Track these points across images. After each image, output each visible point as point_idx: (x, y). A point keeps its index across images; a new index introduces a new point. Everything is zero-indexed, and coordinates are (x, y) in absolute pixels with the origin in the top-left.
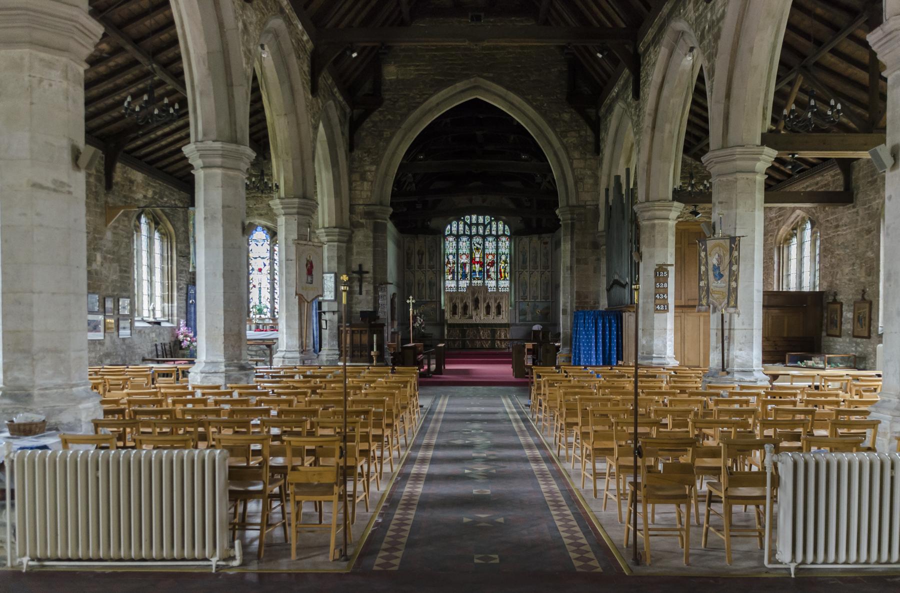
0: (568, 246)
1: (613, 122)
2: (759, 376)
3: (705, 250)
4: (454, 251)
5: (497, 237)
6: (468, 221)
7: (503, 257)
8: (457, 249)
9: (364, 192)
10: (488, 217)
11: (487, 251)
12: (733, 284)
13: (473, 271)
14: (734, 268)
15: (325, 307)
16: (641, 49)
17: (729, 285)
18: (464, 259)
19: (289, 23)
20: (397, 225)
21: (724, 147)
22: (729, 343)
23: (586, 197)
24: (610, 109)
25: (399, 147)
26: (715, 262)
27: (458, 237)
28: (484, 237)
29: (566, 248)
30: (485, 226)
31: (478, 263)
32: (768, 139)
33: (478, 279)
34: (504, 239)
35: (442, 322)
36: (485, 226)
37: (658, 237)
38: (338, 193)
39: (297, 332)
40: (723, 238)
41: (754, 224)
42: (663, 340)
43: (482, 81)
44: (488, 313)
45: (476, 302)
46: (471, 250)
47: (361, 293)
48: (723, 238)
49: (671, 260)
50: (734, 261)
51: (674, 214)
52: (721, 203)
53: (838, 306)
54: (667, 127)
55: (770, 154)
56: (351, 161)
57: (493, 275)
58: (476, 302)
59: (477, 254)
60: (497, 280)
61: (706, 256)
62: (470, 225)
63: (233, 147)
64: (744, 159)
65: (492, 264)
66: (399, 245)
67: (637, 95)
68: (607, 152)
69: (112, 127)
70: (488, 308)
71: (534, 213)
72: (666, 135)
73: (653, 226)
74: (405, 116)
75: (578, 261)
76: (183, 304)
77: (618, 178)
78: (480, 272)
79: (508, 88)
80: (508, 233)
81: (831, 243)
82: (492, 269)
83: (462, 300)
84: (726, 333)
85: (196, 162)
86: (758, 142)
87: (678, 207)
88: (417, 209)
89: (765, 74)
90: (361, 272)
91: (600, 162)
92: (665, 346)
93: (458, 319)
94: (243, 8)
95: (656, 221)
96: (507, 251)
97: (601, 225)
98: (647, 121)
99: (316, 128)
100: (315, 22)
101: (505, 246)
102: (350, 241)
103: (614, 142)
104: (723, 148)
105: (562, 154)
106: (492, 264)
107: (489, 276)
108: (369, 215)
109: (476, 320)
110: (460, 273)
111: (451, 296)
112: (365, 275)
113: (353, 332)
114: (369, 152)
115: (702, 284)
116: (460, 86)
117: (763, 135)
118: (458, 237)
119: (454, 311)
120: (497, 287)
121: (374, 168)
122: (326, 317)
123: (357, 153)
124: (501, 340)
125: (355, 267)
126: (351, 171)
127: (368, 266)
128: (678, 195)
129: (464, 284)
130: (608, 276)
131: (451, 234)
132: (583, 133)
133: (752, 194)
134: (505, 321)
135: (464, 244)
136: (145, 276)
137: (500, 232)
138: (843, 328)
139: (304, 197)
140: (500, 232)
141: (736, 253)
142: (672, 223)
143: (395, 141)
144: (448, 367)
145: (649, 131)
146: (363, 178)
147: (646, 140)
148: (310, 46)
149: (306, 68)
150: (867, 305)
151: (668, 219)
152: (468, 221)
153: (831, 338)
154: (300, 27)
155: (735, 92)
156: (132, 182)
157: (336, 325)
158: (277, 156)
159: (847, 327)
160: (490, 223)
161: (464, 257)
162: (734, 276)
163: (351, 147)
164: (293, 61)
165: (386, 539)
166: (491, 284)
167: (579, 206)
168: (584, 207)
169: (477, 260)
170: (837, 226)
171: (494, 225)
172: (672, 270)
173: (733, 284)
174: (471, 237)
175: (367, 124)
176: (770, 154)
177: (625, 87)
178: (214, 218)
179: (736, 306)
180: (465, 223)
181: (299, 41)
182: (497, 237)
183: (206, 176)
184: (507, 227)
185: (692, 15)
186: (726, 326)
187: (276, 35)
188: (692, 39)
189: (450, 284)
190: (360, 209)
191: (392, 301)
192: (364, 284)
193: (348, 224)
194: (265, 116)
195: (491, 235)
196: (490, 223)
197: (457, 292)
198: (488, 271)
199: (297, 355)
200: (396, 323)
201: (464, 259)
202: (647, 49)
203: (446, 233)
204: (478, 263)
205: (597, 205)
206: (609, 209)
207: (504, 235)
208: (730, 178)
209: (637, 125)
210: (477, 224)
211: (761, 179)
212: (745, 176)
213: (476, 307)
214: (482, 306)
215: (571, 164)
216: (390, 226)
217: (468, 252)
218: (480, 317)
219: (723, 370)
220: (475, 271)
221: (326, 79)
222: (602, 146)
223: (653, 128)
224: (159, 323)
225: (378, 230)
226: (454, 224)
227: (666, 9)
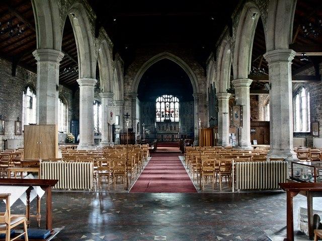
0: (197, 107)
2: (250, 147)
9: (129, 89)
13: (166, 114)
16: (216, 46)
18: (163, 110)
19: (107, 40)
20: (139, 99)
21: (237, 78)
23: (202, 90)
24: (209, 63)
27: (161, 102)
28: (170, 102)
29: (196, 107)
30: (170, 99)
32: (250, 77)
36: (170, 99)
37: (223, 104)
38: (120, 90)
40: (238, 105)
42: (227, 138)
43: (168, 53)
44: (171, 129)
48: (238, 105)
50: (241, 113)
54: (225, 70)
55: (250, 81)
56: (124, 79)
57: (173, 116)
59: (167, 106)
62: (165, 99)
63: (92, 79)
65: (173, 112)
66: (140, 105)
67: (215, 60)
68: (208, 76)
69: (70, 82)
71: (186, 96)
72: (224, 72)
73: (222, 101)
74: (142, 64)
76: (70, 126)
77: (211, 84)
79: (176, 55)
80: (178, 101)
82: (173, 114)
85: (37, 58)
86: (247, 77)
88: (146, 95)
89: (247, 58)
91: (206, 80)
94: (95, 40)
98: (219, 68)
99: (114, 70)
101: (177, 105)
102: (124, 105)
105: (194, 76)
106: (173, 112)
107: (172, 116)
108: (130, 96)
110: (161, 115)
114: (130, 76)
117: (248, 75)
118: (161, 102)
123: (126, 76)
124: (176, 139)
125: (126, 114)
126: (124, 82)
127: (130, 113)
128: (229, 91)
135: (163, 104)
136: (100, 121)
139: (110, 92)
141: (242, 110)
142: (228, 100)
144: (158, 148)
146: (128, 84)
147: (219, 74)
150: (317, 123)
155: (240, 63)
158: (102, 79)
162: (241, 117)
163: (125, 74)
164: (108, 51)
167: (200, 93)
171: (173, 98)
174: (165, 102)
176: (250, 81)
177: (212, 57)
178: (85, 100)
179: (242, 126)
183: (83, 89)
185: (228, 40)
187: (103, 45)
188: (228, 46)
189: (158, 119)
190: (127, 94)
193: (123, 100)
199: (107, 142)
208: (239, 88)
209: (216, 68)
210: (167, 98)
211: (248, 88)
215: (197, 79)
216: (137, 100)
221: (117, 55)
223: (221, 70)
224: (63, 132)
225: (133, 101)
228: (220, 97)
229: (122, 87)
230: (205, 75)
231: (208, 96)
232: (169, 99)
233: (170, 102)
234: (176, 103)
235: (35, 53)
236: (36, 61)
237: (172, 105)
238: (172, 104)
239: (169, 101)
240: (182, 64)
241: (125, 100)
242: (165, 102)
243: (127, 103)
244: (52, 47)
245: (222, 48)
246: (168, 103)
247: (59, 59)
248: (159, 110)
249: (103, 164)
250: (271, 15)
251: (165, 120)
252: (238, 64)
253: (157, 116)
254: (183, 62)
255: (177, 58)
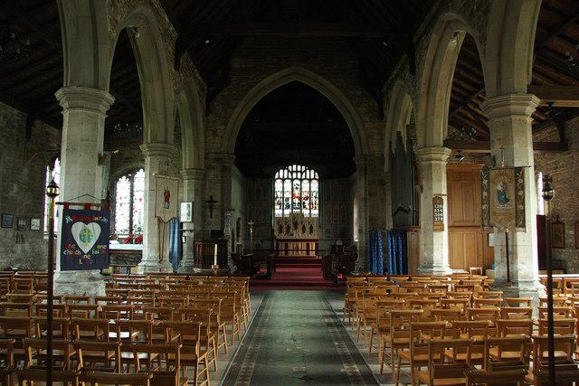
0: (362, 184)
1: (393, 95)
3: (488, 178)
5: (310, 180)
7: (314, 194)
10: (304, 167)
12: (521, 207)
13: (293, 203)
14: (521, 193)
15: (185, 228)
16: (415, 40)
17: (516, 208)
18: (288, 195)
21: (499, 94)
22: (512, 257)
24: (390, 87)
25: (240, 113)
26: (499, 188)
27: (283, 180)
28: (301, 180)
35: (272, 238)
38: (196, 144)
39: (157, 246)
41: (527, 157)
42: (441, 253)
44: (311, 232)
45: (296, 224)
46: (292, 188)
47: (211, 217)
49: (444, 191)
51: (445, 157)
52: (498, 140)
53: (561, 226)
54: (438, 92)
55: (535, 101)
57: (308, 206)
58: (296, 224)
59: (296, 190)
60: (310, 209)
61: (488, 183)
63: (94, 91)
64: (517, 104)
67: (413, 71)
68: (389, 116)
70: (304, 228)
74: (246, 91)
75: (370, 194)
81: (103, 258)
83: (286, 223)
84: (510, 249)
85: (65, 104)
87: (448, 151)
90: (211, 201)
91: (384, 125)
92: (442, 257)
93: (283, 236)
95: (433, 162)
96: (317, 190)
97: (386, 168)
98: (423, 89)
100: (180, 20)
101: (315, 186)
102: (204, 179)
103: (395, 109)
104: (497, 96)
106: (306, 198)
107: (304, 207)
108: (218, 160)
109: (296, 236)
111: (279, 220)
112: (215, 204)
113: (204, 246)
115: (484, 207)
116: (285, 72)
118: (283, 180)
119: (280, 231)
120: (310, 214)
121: (222, 127)
122: (185, 234)
123: (211, 117)
125: (207, 198)
126: (206, 130)
127: (217, 197)
129: (287, 212)
130: (394, 202)
131: (279, 178)
132: (371, 104)
133: (524, 132)
134: (316, 237)
135: (288, 183)
137: (312, 177)
138: (567, 242)
142: (444, 164)
143: (238, 110)
145: (425, 95)
148: (175, 35)
149: (171, 49)
151: (441, 160)
153: (556, 250)
154: (167, 19)
156: (48, 134)
157: (192, 240)
159: (570, 241)
160: (305, 171)
163: (207, 112)
165: (242, 370)
166: (306, 212)
168: (373, 155)
170: (556, 168)
171: (308, 171)
172: (445, 198)
173: (521, 207)
174: (292, 180)
175: (219, 97)
176: (535, 101)
180: (289, 171)
181: (166, 30)
182: (310, 180)
186: (510, 243)
189: (278, 212)
190: (212, 156)
191: (238, 223)
192: (214, 210)
194: (139, 84)
195: (305, 179)
196: (305, 171)
197: (283, 218)
200: (240, 238)
202: (420, 38)
203: (276, 177)
205: (383, 155)
206: (392, 157)
207: (315, 179)
208: (506, 119)
210: (297, 172)
211: (530, 120)
212: (518, 117)
213: (296, 228)
214: (300, 227)
216: (235, 169)
218: (298, 234)
219: (509, 280)
222: (385, 112)
225: (225, 170)
226: (281, 171)
227: (434, 8)
228: (425, 157)
229: (202, 137)
230: (382, 116)
231: (387, 161)
232: (299, 174)
233: (301, 180)
234: (314, 181)
235: (59, 94)
236: (62, 109)
237: (305, 185)
238: (305, 185)
239: (299, 177)
240: (331, 91)
241: (209, 167)
242: (292, 180)
243: (211, 174)
244: (91, 80)
245: (434, 37)
246: (298, 182)
247: (104, 108)
248: (279, 195)
249: (307, 202)
250: (492, 32)
251: (291, 214)
252: (500, 54)
253: (277, 207)
254: (332, 87)
255: (321, 79)
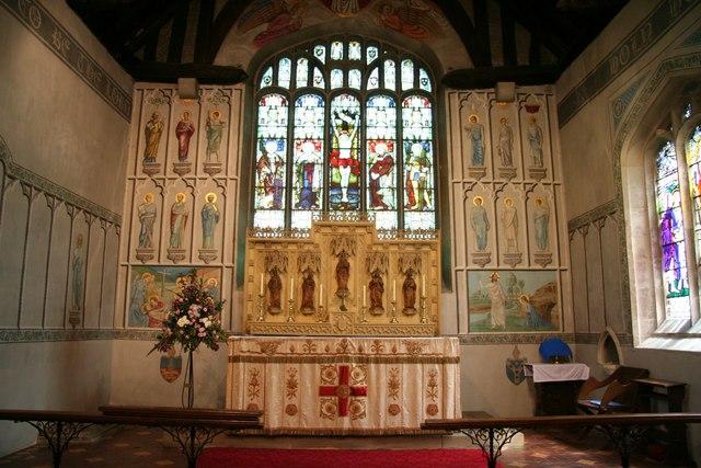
4: (283, 132)
5: (399, 98)
6: (322, 59)
7: (417, 150)
8: (291, 127)
11: (371, 133)
13: (330, 186)
18: (308, 153)
27: (292, 96)
28: (363, 96)
31: (346, 163)
33: (347, 207)
34: (416, 102)
46: (328, 127)
57: (389, 198)
60: (400, 211)
78: (351, 187)
82: (387, 181)
106: (384, 166)
107: (377, 200)
118: (292, 96)
131: (275, 89)
137: (302, 83)
140: (407, 85)
152: (322, 59)
161: (308, 147)
169: (345, 154)
174: (327, 96)
182: (399, 98)
184: (423, 74)
195: (381, 91)
196: (379, 64)
198: (375, 186)
201: (308, 153)
203: (263, 85)
204: (346, 163)
207: (416, 91)
217: (319, 133)
220: (337, 186)
237: (381, 117)
249: (387, 181)
